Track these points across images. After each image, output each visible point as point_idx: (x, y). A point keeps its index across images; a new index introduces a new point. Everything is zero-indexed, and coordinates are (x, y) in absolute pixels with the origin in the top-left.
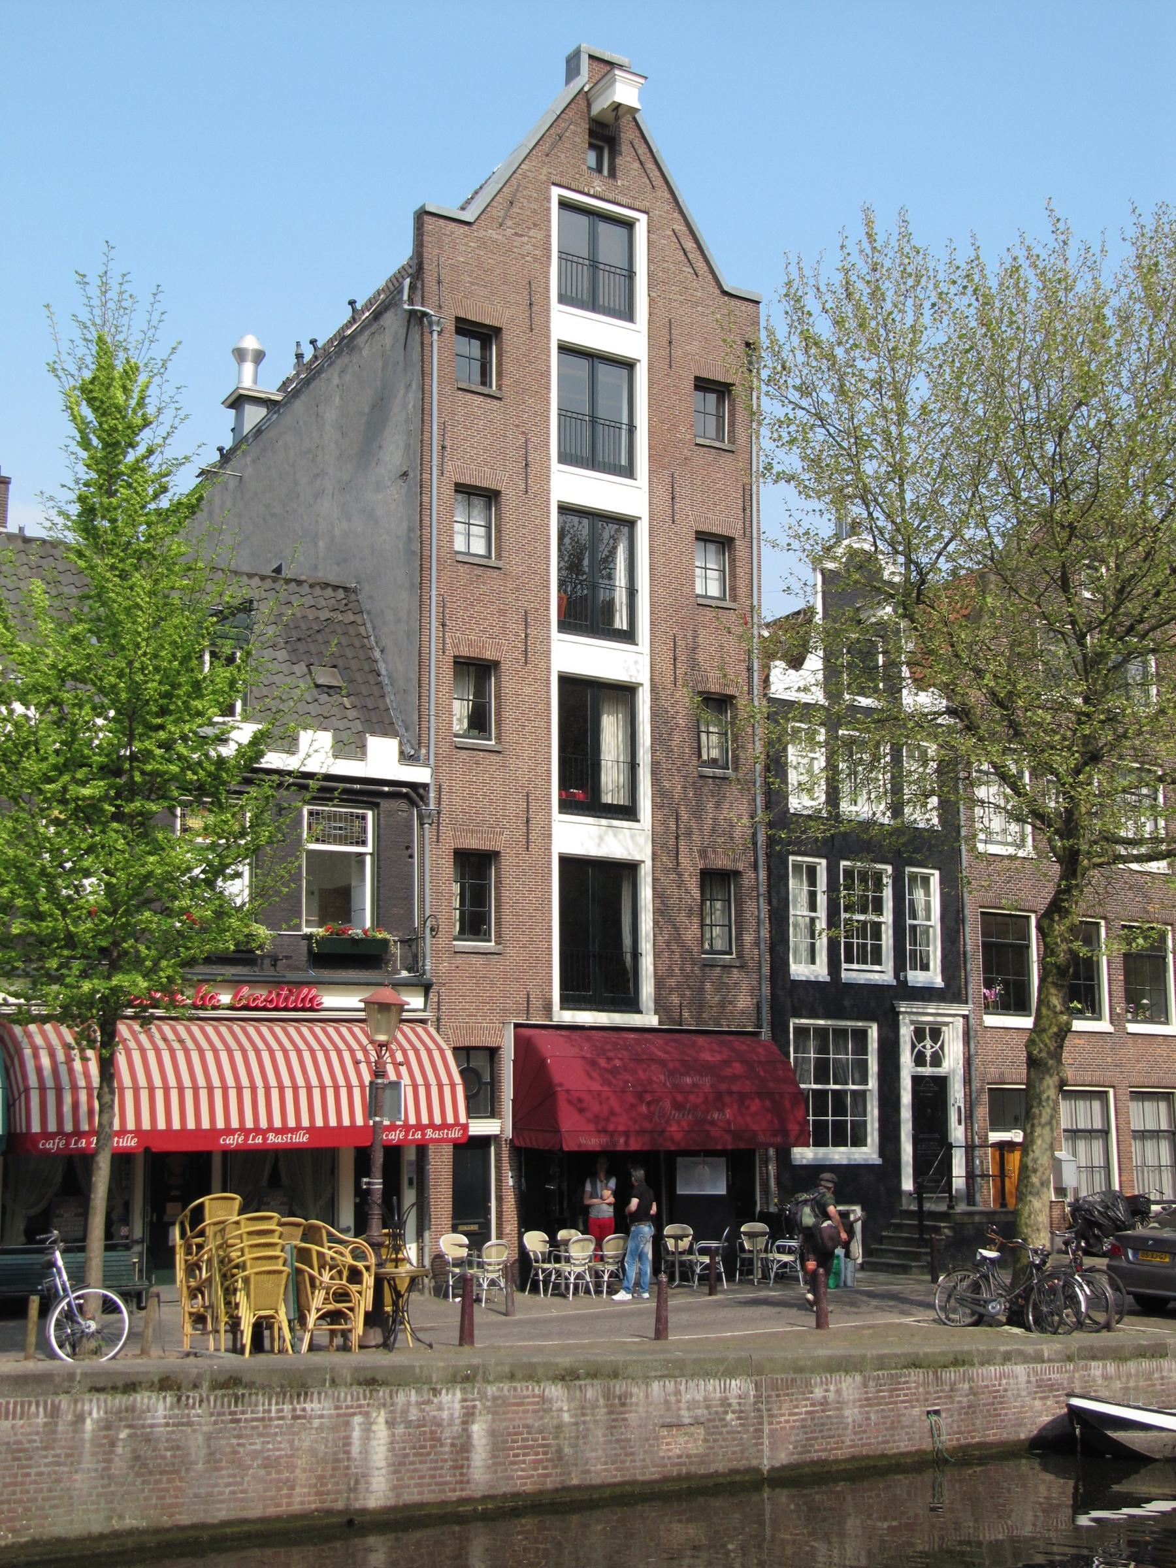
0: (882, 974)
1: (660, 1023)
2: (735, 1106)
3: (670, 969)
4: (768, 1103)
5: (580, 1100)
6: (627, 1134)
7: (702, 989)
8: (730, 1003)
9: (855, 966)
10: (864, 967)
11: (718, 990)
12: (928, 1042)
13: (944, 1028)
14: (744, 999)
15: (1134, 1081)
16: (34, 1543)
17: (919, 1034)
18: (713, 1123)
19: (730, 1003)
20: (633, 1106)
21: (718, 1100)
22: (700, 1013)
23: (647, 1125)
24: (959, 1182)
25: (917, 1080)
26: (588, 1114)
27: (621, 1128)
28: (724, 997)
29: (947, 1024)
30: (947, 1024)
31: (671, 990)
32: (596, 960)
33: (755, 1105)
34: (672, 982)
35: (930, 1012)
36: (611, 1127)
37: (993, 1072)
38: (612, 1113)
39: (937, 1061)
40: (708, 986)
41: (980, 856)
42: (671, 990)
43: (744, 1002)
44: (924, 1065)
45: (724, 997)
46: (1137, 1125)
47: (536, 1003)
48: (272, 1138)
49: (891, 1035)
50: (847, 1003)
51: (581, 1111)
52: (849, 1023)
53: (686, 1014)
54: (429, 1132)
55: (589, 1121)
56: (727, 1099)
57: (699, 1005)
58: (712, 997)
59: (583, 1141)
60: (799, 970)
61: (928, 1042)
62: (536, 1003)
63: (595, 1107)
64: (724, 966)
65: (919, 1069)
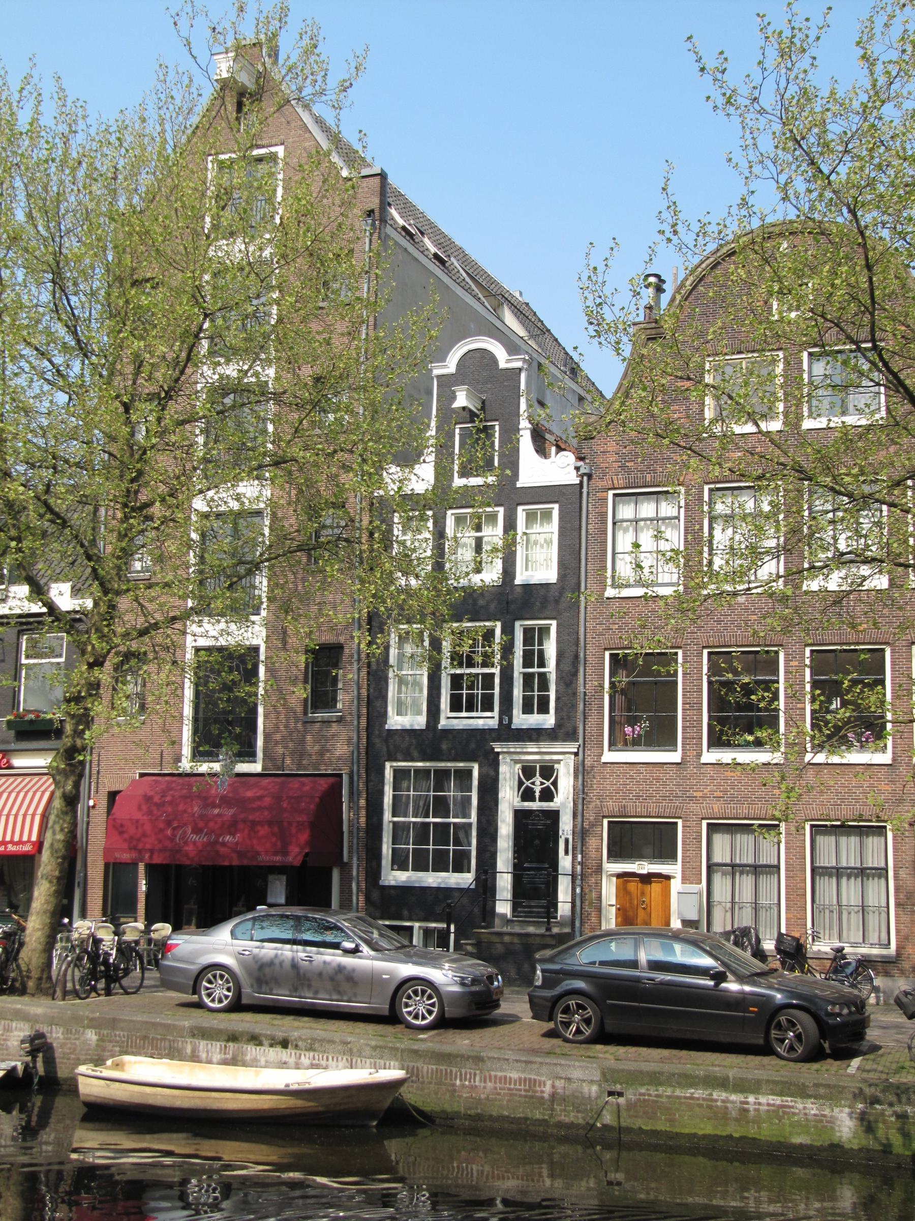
0: (487, 720)
1: (263, 769)
2: (246, 831)
3: (277, 726)
4: (276, 829)
5: (122, 826)
6: (152, 851)
7: (303, 741)
8: (328, 751)
9: (464, 714)
10: (474, 714)
11: (316, 741)
12: (538, 779)
13: (556, 766)
14: (341, 748)
15: (814, 814)
16: (404, 1136)
17: (528, 771)
18: (224, 844)
19: (328, 751)
20: (161, 830)
21: (232, 827)
22: (300, 760)
23: (168, 844)
24: (564, 908)
25: (520, 815)
26: (126, 836)
27: (148, 846)
28: (323, 747)
29: (558, 762)
30: (558, 762)
31: (277, 743)
32: (224, 723)
33: (263, 831)
34: (278, 737)
35: (533, 752)
36: (140, 846)
37: (611, 805)
38: (144, 835)
39: (547, 795)
40: (309, 738)
41: (604, 602)
42: (277, 743)
43: (341, 749)
44: (533, 800)
45: (323, 747)
46: (827, 860)
47: (167, 757)
48: (10, 848)
49: (492, 773)
50: (444, 746)
51: (121, 833)
52: (449, 764)
53: (288, 761)
54: (10, 846)
55: (125, 840)
56: (241, 826)
57: (300, 754)
58: (312, 747)
59: (117, 855)
60: (396, 721)
61: (538, 779)
62: (167, 757)
63: (132, 830)
64: (324, 722)
65: (526, 804)
